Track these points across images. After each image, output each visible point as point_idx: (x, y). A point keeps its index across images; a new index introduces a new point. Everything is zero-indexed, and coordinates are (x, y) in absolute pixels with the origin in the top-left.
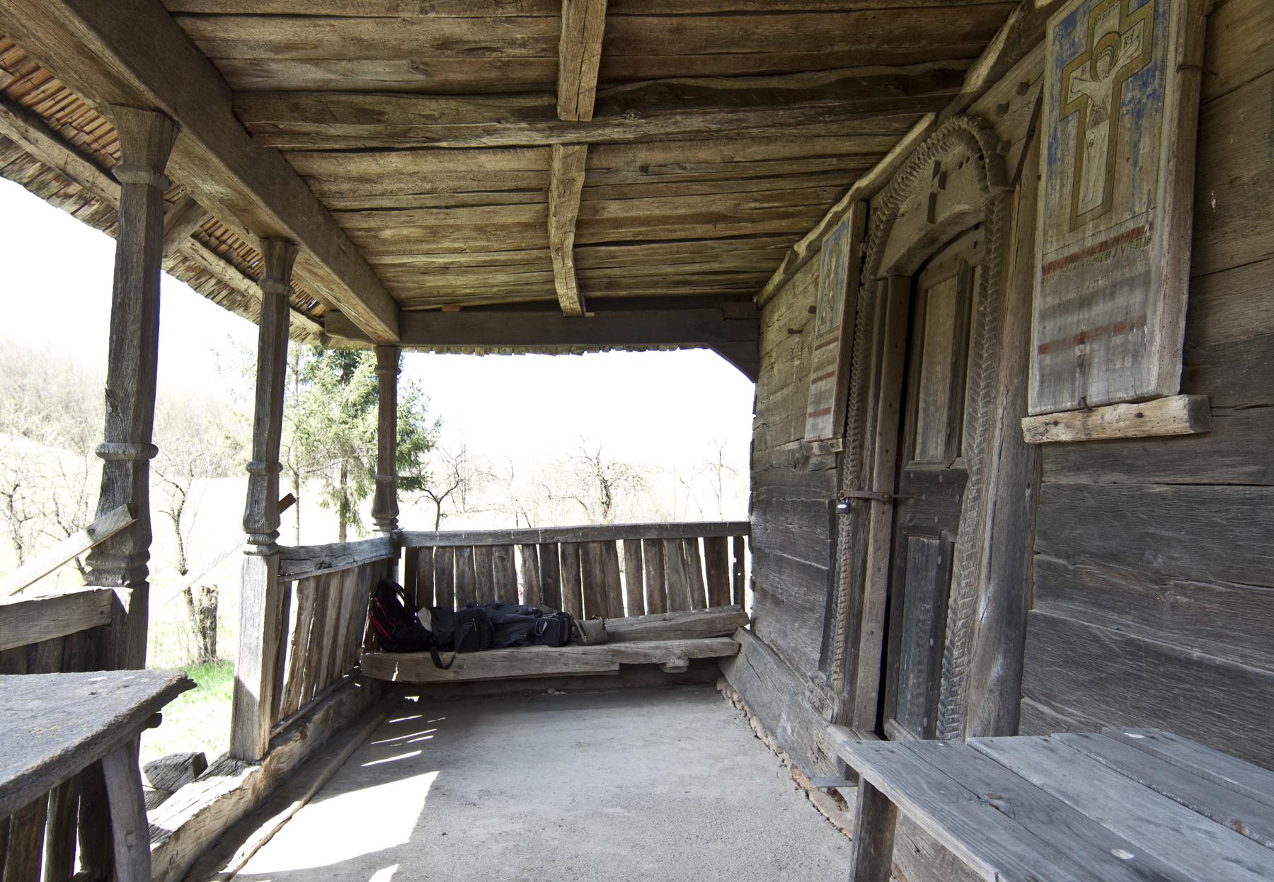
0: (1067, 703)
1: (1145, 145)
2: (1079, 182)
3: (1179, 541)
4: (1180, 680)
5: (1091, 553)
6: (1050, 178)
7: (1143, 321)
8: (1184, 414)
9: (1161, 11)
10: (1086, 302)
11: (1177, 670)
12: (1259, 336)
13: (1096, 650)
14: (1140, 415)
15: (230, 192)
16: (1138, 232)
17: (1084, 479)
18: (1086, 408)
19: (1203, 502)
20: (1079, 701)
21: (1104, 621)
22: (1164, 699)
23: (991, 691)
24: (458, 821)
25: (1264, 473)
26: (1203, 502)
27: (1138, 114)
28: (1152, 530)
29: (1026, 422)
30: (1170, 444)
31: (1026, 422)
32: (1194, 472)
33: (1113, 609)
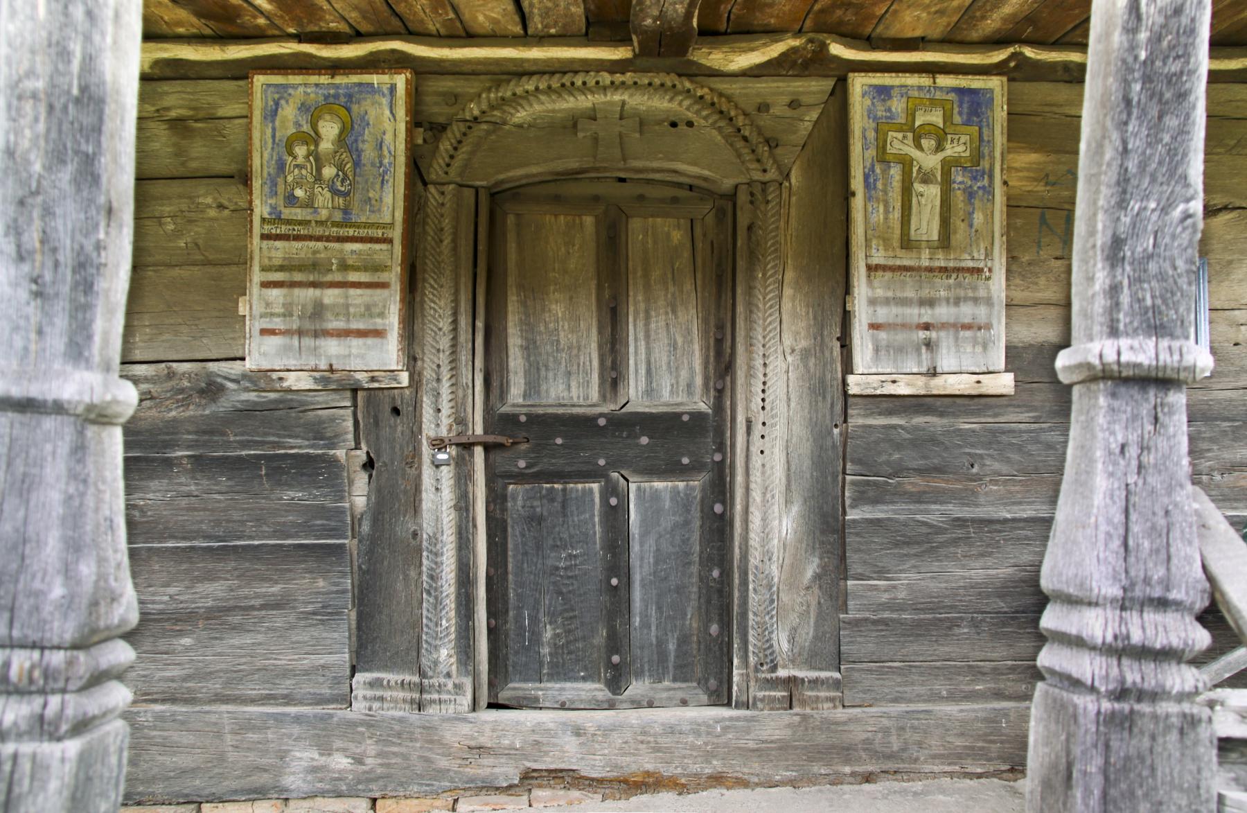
0: (901, 571)
1: (978, 218)
2: (909, 215)
3: (989, 455)
4: (1000, 531)
5: (914, 470)
6: (868, 198)
7: (988, 327)
8: (1012, 383)
9: (986, 138)
10: (931, 303)
11: (998, 527)
12: (1031, 345)
13: (924, 530)
14: (979, 382)
15: (798, 163)
16: (979, 271)
17: (895, 421)
18: (933, 373)
19: (1004, 433)
20: (915, 567)
21: (927, 512)
22: (988, 546)
23: (808, 588)
24: (1026, 557)
25: (1040, 417)
26: (1004, 433)
27: (970, 195)
28: (967, 450)
29: (851, 379)
30: (976, 400)
31: (851, 379)
32: (996, 415)
33: (935, 503)
